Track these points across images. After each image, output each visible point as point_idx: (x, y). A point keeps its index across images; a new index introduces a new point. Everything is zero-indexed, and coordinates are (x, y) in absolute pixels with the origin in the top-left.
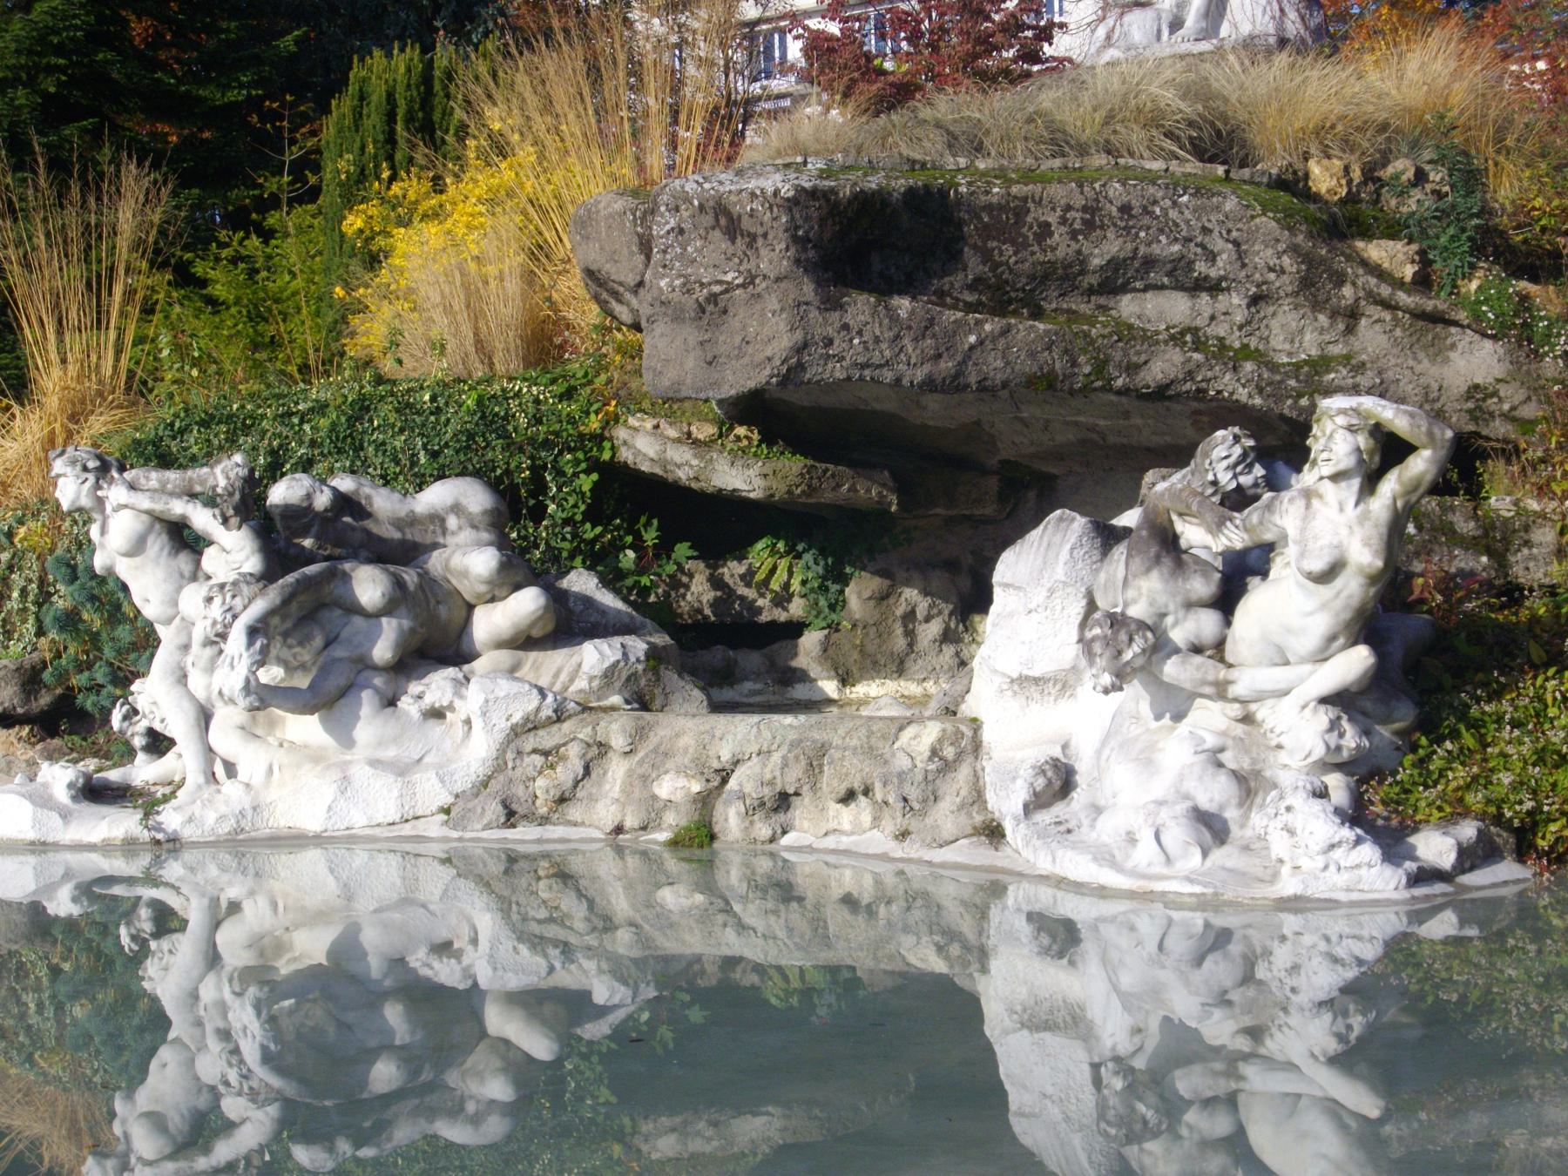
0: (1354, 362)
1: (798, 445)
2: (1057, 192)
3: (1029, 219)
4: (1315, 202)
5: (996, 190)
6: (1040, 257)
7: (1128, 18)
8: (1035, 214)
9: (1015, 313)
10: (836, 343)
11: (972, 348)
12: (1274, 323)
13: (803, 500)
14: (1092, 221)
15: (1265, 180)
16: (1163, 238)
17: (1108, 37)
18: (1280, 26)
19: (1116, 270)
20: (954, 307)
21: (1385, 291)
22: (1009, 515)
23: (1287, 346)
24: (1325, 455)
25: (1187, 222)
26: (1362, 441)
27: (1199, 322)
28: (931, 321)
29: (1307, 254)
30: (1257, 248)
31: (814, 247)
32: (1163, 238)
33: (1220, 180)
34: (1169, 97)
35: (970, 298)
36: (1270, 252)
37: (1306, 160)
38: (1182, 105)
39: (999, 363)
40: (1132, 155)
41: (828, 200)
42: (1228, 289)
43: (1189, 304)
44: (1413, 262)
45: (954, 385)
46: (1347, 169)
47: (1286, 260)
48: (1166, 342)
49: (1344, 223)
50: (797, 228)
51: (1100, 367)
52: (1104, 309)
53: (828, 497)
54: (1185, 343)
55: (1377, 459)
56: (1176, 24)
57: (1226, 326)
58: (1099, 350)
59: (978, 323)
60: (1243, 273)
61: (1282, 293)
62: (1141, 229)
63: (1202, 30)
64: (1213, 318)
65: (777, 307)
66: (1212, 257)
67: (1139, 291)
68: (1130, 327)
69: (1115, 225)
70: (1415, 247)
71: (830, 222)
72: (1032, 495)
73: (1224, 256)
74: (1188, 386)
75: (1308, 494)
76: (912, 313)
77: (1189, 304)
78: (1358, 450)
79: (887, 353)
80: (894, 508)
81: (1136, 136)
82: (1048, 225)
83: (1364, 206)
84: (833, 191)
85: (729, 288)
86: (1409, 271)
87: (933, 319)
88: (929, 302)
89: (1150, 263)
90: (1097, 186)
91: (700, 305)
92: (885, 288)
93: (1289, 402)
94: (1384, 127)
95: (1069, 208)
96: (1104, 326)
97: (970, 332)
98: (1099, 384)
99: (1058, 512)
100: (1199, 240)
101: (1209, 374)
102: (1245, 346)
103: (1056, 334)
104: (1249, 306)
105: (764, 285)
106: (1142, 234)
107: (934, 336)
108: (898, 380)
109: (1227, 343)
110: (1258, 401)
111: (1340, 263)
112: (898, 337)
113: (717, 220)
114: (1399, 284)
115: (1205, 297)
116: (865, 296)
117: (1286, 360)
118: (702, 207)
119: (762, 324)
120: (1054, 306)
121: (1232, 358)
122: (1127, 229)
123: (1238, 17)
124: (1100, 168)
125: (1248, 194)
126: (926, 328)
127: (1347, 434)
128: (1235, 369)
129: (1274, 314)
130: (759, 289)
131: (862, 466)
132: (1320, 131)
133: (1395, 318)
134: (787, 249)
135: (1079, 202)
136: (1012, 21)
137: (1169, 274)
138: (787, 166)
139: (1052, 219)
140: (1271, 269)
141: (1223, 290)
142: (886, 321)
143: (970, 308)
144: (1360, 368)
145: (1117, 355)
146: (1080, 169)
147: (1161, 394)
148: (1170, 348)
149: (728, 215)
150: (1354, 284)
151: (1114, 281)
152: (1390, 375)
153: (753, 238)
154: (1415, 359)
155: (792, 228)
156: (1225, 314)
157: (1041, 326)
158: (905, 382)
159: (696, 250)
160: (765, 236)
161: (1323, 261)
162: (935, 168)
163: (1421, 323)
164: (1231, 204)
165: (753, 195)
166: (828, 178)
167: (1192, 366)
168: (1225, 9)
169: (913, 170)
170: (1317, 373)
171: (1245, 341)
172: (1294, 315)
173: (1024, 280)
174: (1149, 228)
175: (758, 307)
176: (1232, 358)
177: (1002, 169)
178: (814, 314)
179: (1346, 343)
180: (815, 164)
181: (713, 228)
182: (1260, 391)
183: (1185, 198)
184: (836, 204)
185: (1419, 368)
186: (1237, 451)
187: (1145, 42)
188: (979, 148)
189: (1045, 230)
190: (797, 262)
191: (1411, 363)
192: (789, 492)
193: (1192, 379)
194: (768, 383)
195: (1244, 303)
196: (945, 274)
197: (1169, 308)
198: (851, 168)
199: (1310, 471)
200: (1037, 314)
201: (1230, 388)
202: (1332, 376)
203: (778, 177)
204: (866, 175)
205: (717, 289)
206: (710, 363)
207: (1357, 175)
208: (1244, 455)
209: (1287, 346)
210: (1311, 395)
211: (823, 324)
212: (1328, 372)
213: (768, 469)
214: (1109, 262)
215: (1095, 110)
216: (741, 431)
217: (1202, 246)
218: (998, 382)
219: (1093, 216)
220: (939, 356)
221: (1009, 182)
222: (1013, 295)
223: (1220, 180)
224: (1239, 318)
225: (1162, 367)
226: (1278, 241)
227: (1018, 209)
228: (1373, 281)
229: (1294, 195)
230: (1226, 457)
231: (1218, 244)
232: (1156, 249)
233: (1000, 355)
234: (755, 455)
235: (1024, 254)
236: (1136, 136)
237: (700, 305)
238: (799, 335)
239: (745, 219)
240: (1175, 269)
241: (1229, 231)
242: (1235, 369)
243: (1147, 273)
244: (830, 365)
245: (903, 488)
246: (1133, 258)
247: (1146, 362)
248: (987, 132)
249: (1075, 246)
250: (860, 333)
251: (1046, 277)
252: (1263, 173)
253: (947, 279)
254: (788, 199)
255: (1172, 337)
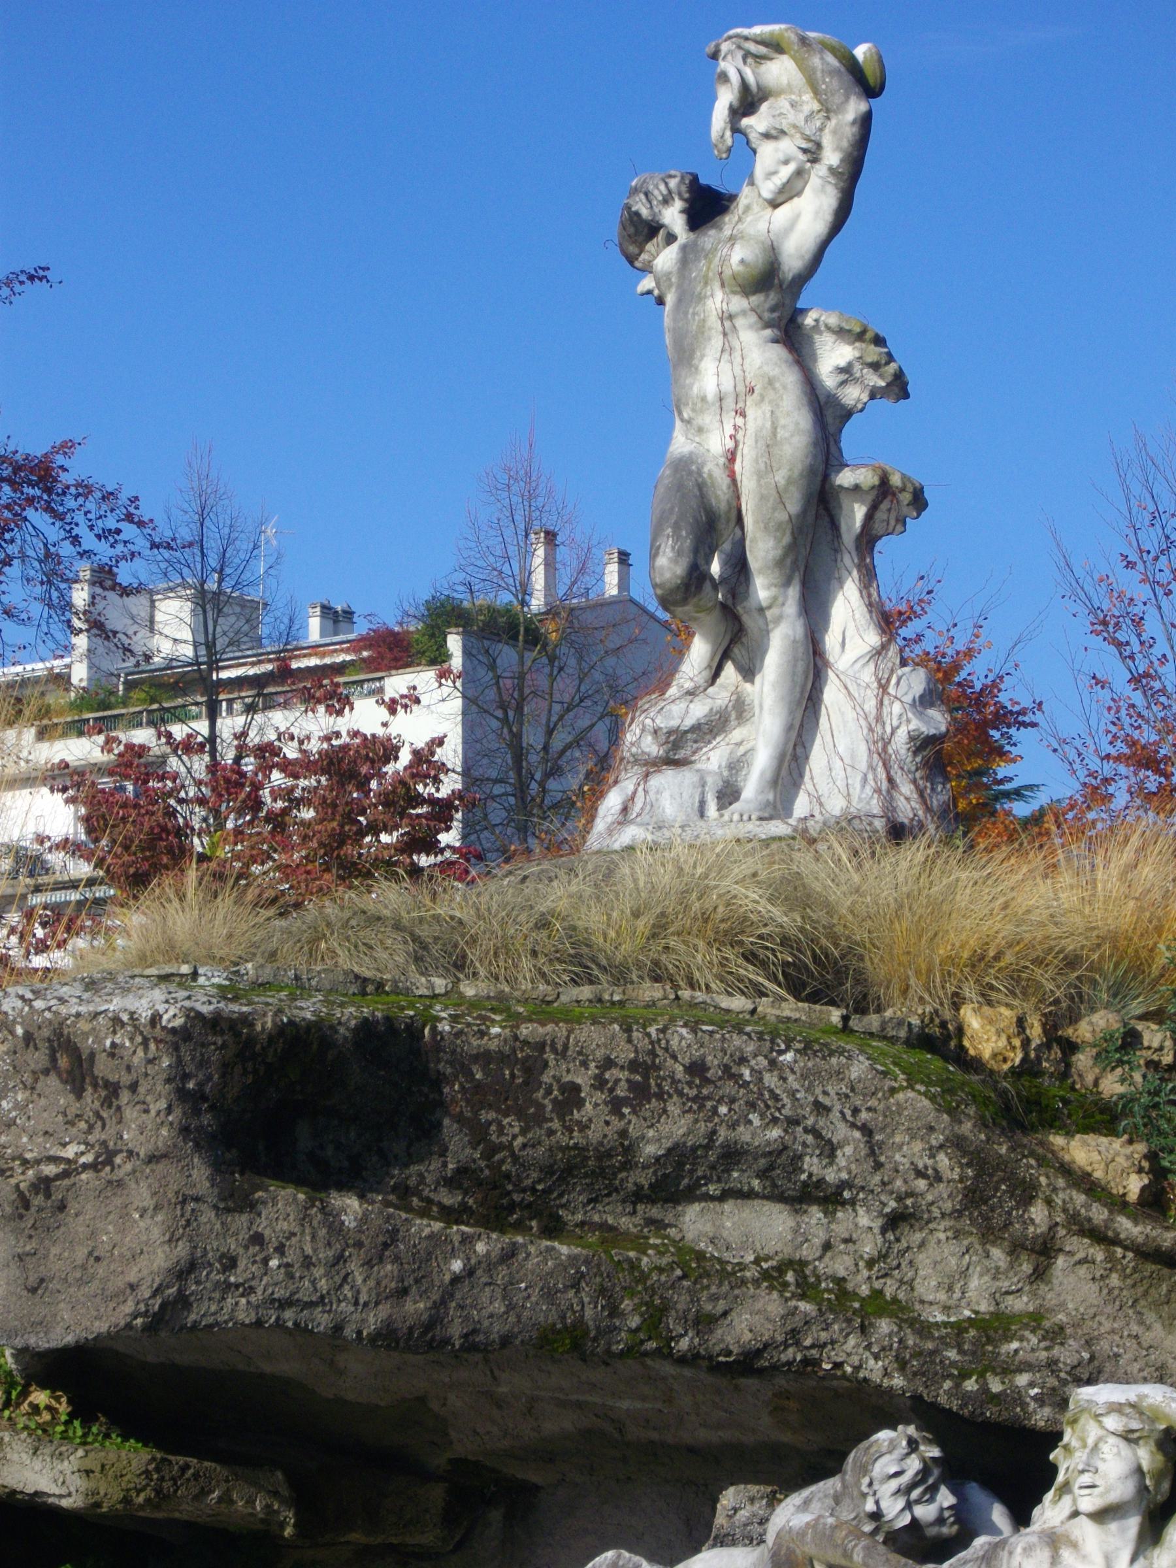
0: (1047, 1324)
1: (132, 1425)
2: (590, 1036)
3: (546, 1078)
4: (976, 1072)
5: (495, 1030)
6: (562, 1138)
7: (655, 781)
8: (555, 1071)
9: (519, 1227)
10: (242, 1263)
11: (456, 1280)
12: (922, 1259)
13: (146, 1513)
14: (645, 1085)
15: (903, 1034)
16: (754, 1118)
17: (625, 810)
18: (889, 808)
19: (680, 1165)
20: (424, 1213)
21: (1099, 1214)
22: (459, 1546)
23: (942, 1296)
24: (1086, 1479)
25: (792, 1094)
26: (1146, 1456)
27: (806, 1252)
28: (393, 1235)
29: (978, 1151)
30: (898, 1139)
31: (212, 1108)
32: (754, 1118)
33: (835, 1031)
34: (753, 900)
35: (449, 1199)
36: (918, 1146)
37: (956, 1007)
38: (777, 912)
39: (498, 1307)
40: (692, 984)
41: (237, 1034)
42: (853, 1202)
43: (791, 1223)
44: (1140, 1171)
45: (426, 1339)
46: (1021, 1022)
47: (943, 1161)
48: (756, 1283)
49: (1027, 1104)
50: (186, 1077)
51: (655, 1317)
52: (658, 1225)
53: (185, 1510)
54: (786, 1285)
55: (1166, 1486)
56: (728, 794)
57: (848, 1261)
58: (652, 1291)
59: (466, 1240)
60: (877, 1179)
61: (936, 1212)
62: (720, 1101)
63: (768, 804)
64: (827, 1246)
65: (149, 1203)
66: (829, 1150)
67: (712, 1198)
68: (700, 1256)
69: (681, 1094)
70: (1141, 1148)
71: (238, 1069)
72: (496, 1515)
73: (848, 1150)
74: (790, 1353)
75: (1054, 1541)
76: (364, 1219)
77: (791, 1223)
78: (1139, 1470)
79: (323, 1284)
80: (288, 1532)
81: (702, 958)
82: (576, 1088)
83: (1046, 1081)
84: (245, 1020)
85: (71, 1169)
86: (1134, 1185)
87: (395, 1231)
88: (387, 1204)
89: (733, 1155)
90: (652, 1030)
91: (21, 1195)
92: (321, 1178)
93: (947, 1385)
94: (1072, 962)
95: (608, 1063)
96: (661, 1254)
97: (453, 1254)
98: (652, 1345)
99: (610, 1554)
100: (810, 1122)
101: (824, 1336)
102: (878, 1294)
103: (587, 1262)
104: (884, 1231)
105: (128, 1167)
106: (723, 1110)
107: (397, 1259)
108: (338, 1328)
109: (850, 1286)
110: (898, 1381)
111: (1028, 1167)
112: (340, 1259)
113: (54, 1060)
114: (1119, 1204)
115: (816, 1214)
116: (290, 1190)
117: (940, 1318)
118: (28, 1038)
119: (122, 1231)
120: (579, 1217)
121: (862, 1311)
122: (699, 1099)
123: (823, 788)
124: (652, 1004)
125: (883, 1054)
126: (386, 1246)
127: (1122, 1444)
128: (863, 1329)
129: (922, 1245)
130: (120, 1174)
131: (240, 1461)
132: (979, 961)
133: (1110, 1258)
134: (169, 1110)
135: (624, 1054)
136: (401, 791)
137: (762, 1175)
138: (165, 978)
139: (583, 1079)
140: (920, 1174)
141: (843, 1203)
142: (323, 1232)
143: (451, 1215)
144: (1056, 1335)
145: (682, 1301)
146: (621, 1003)
147: (748, 1364)
148: (762, 1292)
149: (73, 1050)
150: (1049, 1202)
151: (677, 1181)
152: (1103, 1346)
153: (113, 1090)
154: (1141, 1323)
155: (178, 1076)
156: (848, 1241)
157: (564, 1250)
158: (349, 1332)
159: (16, 1106)
160: (134, 1087)
161: (1002, 1164)
162: (396, 991)
163: (1150, 1267)
164: (859, 1068)
165: (116, 1021)
166: (235, 999)
167: (797, 1321)
168: (801, 775)
169: (364, 993)
170: (990, 1340)
171: (877, 1285)
172: (954, 1247)
173: (535, 1175)
174: (733, 1101)
175: (118, 1201)
176: (862, 1311)
177: (501, 997)
178: (208, 1215)
179: (1034, 1294)
180: (212, 977)
181: (46, 1072)
182: (902, 1365)
183: (789, 1057)
184: (251, 1041)
185: (1147, 1338)
186: (914, 1465)
187: (681, 818)
188: (460, 965)
189: (571, 1096)
190: (185, 1131)
191: (1135, 1328)
192: (127, 1500)
193: (797, 1343)
194: (129, 1326)
195: (877, 1224)
196: (411, 1159)
197: (763, 1229)
198: (265, 986)
199: (1055, 1502)
200: (554, 1228)
201: (855, 1360)
202: (1015, 1345)
203: (158, 995)
204: (293, 998)
205: (50, 1170)
206: (33, 1290)
207: (1036, 1032)
208: (925, 1472)
209: (942, 1296)
210: (982, 1376)
211: (222, 1233)
212: (1008, 1339)
213: (92, 1463)
214: (670, 1150)
215: (636, 914)
216: (41, 1397)
217: (815, 1132)
218: (494, 1336)
219: (646, 1077)
220: (405, 1291)
221: (515, 1020)
222: (517, 1197)
223: (835, 1031)
224: (868, 1249)
225: (752, 1320)
226: (931, 1129)
227: (530, 1061)
228: (1080, 1198)
229: (946, 1059)
230: (897, 1474)
231: (839, 1131)
232: (744, 1134)
233: (499, 1292)
234: (64, 1436)
235: (537, 1133)
236: (702, 958)
237: (21, 1195)
238: (182, 1250)
239: (101, 1058)
240: (771, 1167)
241: (856, 1111)
242: (863, 1329)
243: (728, 1171)
244: (230, 1301)
245: (303, 1498)
246: (707, 1147)
247: (725, 1314)
248: (474, 940)
249: (617, 1124)
250: (280, 1250)
251: (569, 1170)
252: (900, 1023)
253: (414, 1169)
254: (174, 1031)
255: (766, 1275)
